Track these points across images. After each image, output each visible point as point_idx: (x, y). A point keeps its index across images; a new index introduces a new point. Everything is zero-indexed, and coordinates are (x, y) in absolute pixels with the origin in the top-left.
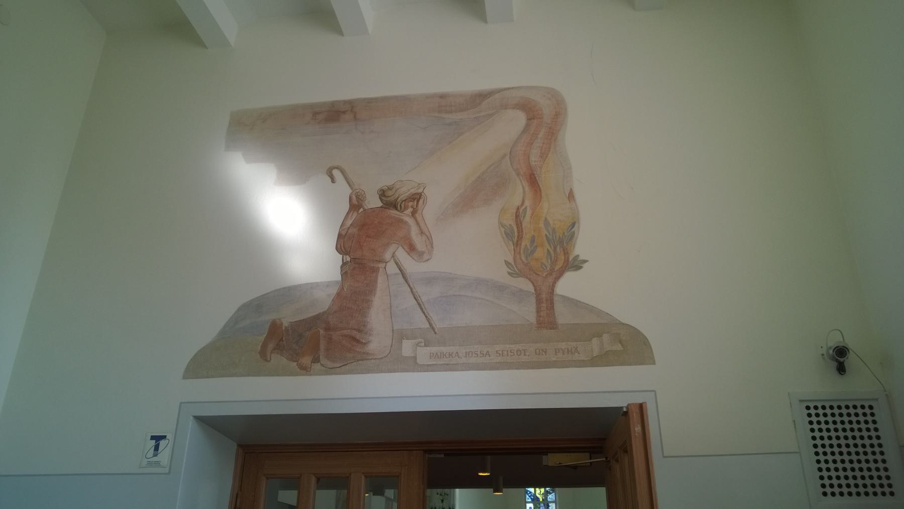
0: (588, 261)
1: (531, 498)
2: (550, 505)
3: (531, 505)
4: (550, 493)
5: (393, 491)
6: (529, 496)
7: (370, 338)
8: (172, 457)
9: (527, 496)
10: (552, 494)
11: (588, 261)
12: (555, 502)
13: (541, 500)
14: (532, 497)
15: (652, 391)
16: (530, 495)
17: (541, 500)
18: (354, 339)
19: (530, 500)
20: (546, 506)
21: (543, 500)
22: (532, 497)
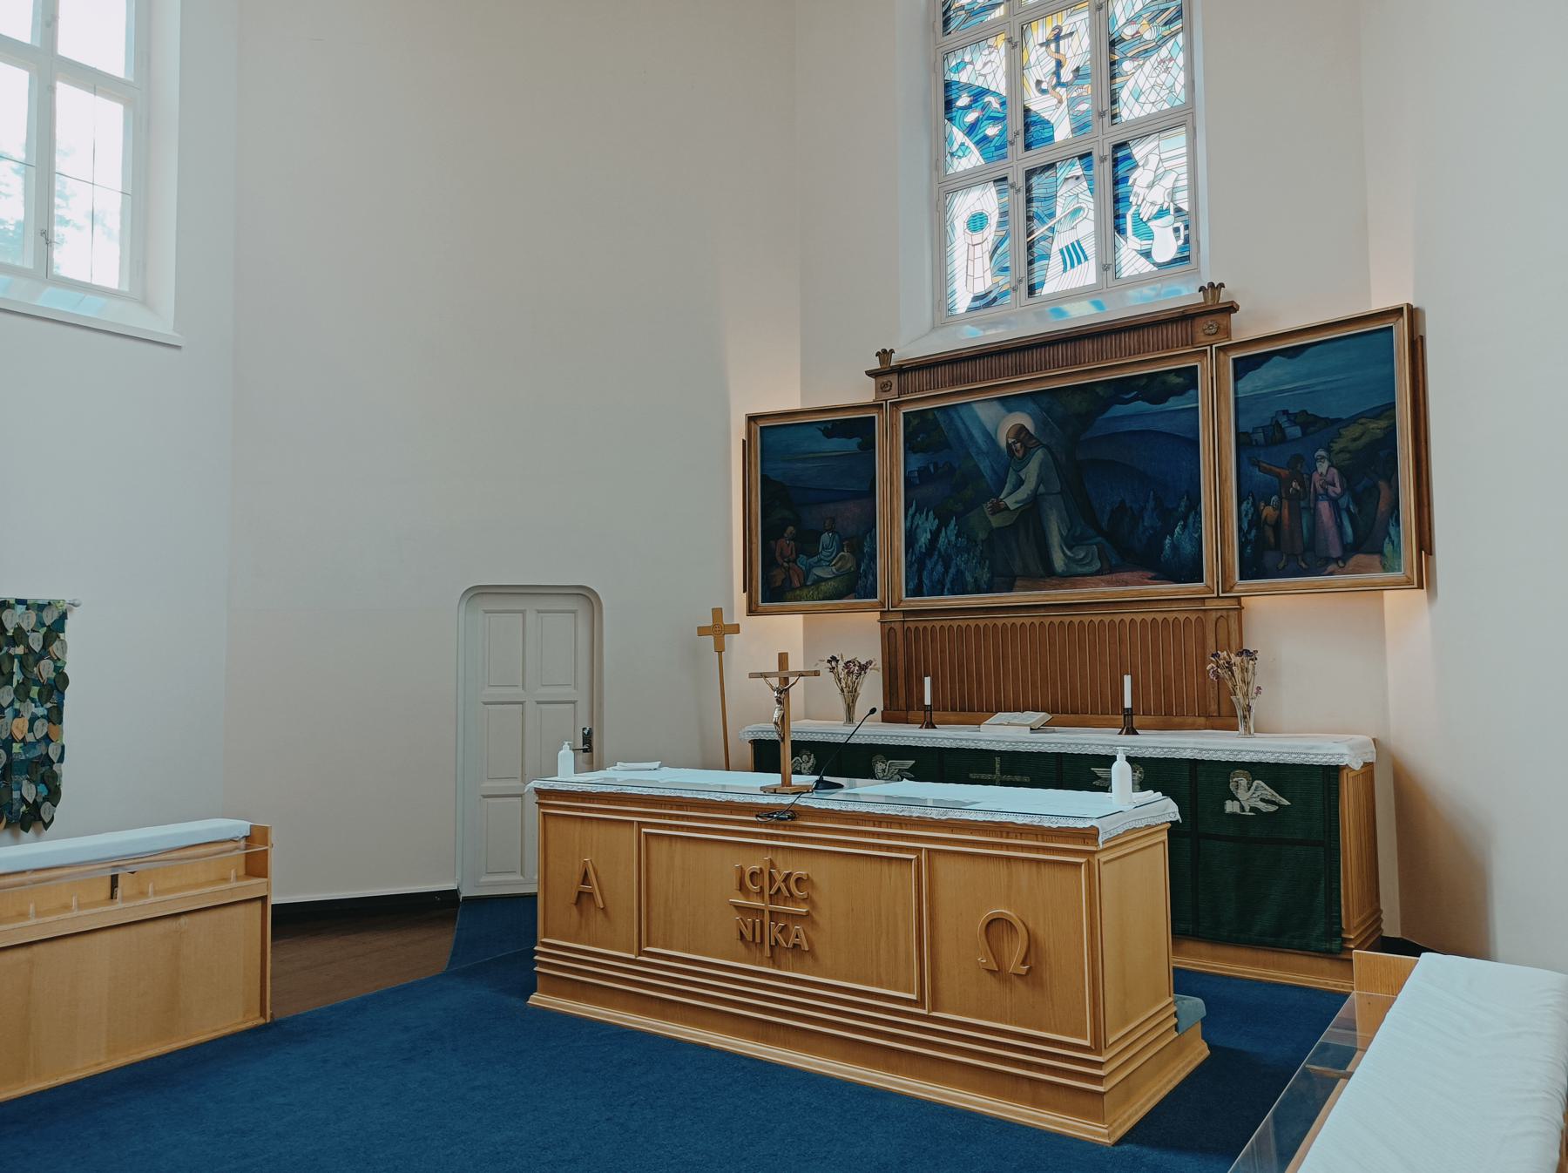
3: (986, 200)
6: (971, 130)
16: (971, 117)
20: (1104, 171)
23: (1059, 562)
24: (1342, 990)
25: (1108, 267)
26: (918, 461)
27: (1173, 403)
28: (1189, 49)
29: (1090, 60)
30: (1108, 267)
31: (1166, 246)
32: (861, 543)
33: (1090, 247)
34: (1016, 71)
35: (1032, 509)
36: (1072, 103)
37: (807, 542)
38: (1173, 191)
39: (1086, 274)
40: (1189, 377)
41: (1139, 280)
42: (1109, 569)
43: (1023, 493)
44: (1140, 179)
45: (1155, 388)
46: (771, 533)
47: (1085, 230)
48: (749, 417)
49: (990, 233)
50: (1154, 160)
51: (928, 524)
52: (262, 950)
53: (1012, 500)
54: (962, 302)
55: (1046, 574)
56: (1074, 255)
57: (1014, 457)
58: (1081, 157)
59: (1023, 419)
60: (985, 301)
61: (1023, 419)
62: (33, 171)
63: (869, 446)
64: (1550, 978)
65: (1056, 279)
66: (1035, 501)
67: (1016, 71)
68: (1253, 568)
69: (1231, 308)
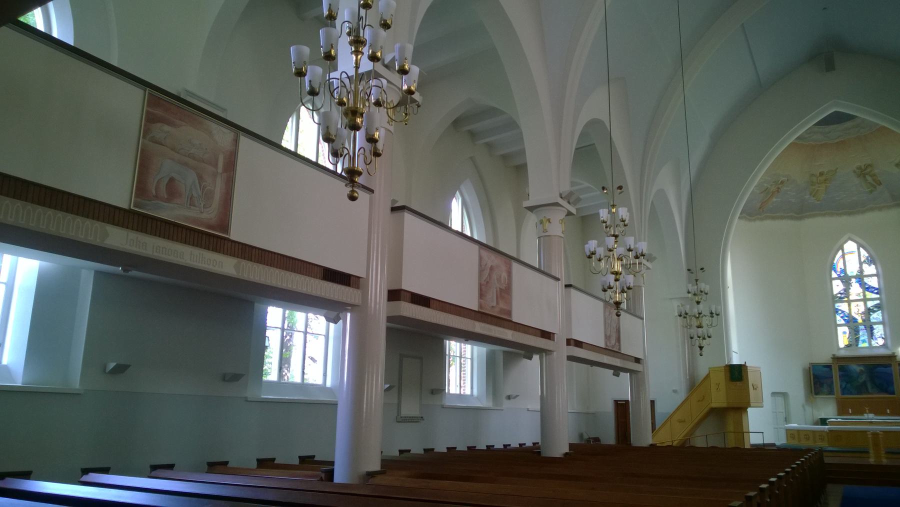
0: (518, 396)
1: (844, 320)
2: (875, 327)
4: (874, 312)
5: (755, 439)
6: (842, 317)
7: (851, 287)
8: (587, 293)
10: (878, 313)
11: (518, 396)
13: (860, 321)
14: (846, 318)
15: (398, 422)
16: (841, 315)
17: (860, 321)
18: (860, 281)
19: (843, 322)
20: (869, 329)
21: (864, 320)
22: (846, 318)
25: (870, 343)
26: (841, 373)
27: (888, 369)
30: (870, 343)
33: (867, 340)
36: (862, 317)
37: (821, 385)
38: (881, 334)
39: (866, 345)
43: (863, 380)
44: (875, 331)
45: (886, 366)
47: (866, 337)
49: (847, 335)
50: (877, 329)
52: (110, 485)
55: (868, 393)
57: (862, 372)
58: (696, 282)
59: (862, 368)
63: (831, 370)
64: (398, 455)
65: (861, 345)
69: (896, 356)
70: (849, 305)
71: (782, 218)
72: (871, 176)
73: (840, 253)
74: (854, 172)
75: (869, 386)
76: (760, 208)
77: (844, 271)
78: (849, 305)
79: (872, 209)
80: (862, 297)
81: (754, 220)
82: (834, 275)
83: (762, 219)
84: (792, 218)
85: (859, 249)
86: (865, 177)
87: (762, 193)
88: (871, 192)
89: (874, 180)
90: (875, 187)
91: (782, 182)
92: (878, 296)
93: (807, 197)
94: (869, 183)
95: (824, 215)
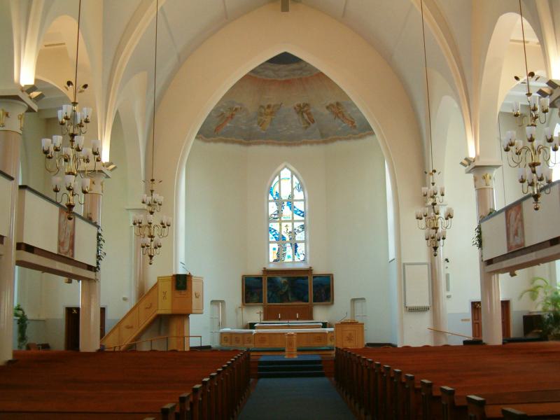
2: (298, 245)
3: (276, 246)
9: (271, 236)
12: (305, 241)
16: (274, 233)
17: (288, 239)
19: (274, 240)
23: (290, 298)
24: (460, 76)
25: (294, 259)
28: (305, 233)
29: (293, 173)
30: (294, 259)
31: (302, 258)
32: (260, 295)
33: (291, 256)
34: (281, 229)
35: (286, 293)
37: (252, 294)
39: (291, 260)
40: (307, 277)
41: (298, 262)
42: (296, 301)
46: (247, 293)
48: (247, 302)
51: (270, 293)
53: (284, 291)
54: (271, 260)
55: (289, 301)
56: (289, 257)
60: (275, 261)
61: (285, 280)
62: (186, 335)
66: (287, 291)
67: (281, 229)
68: (314, 301)
70: (280, 225)
71: (233, 142)
72: (307, 114)
73: (277, 178)
74: (295, 108)
75: (290, 295)
76: (215, 131)
77: (278, 194)
78: (280, 225)
79: (305, 143)
80: (291, 219)
81: (209, 142)
82: (271, 198)
83: (215, 141)
84: (240, 143)
85: (292, 177)
86: (302, 114)
87: (219, 116)
88: (306, 128)
89: (309, 118)
90: (309, 124)
91: (236, 109)
92: (303, 218)
93: (256, 125)
94: (306, 120)
95: (267, 143)
